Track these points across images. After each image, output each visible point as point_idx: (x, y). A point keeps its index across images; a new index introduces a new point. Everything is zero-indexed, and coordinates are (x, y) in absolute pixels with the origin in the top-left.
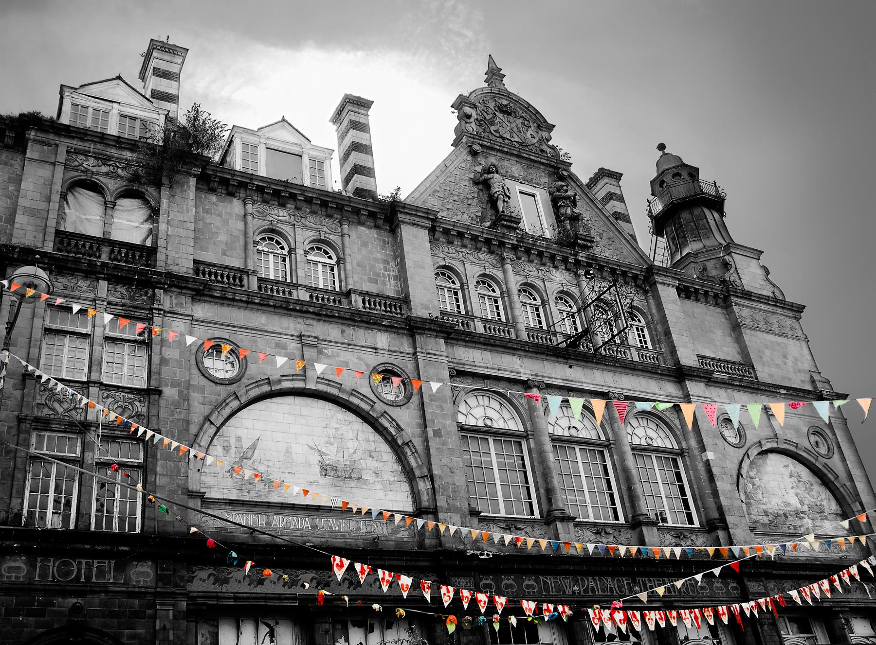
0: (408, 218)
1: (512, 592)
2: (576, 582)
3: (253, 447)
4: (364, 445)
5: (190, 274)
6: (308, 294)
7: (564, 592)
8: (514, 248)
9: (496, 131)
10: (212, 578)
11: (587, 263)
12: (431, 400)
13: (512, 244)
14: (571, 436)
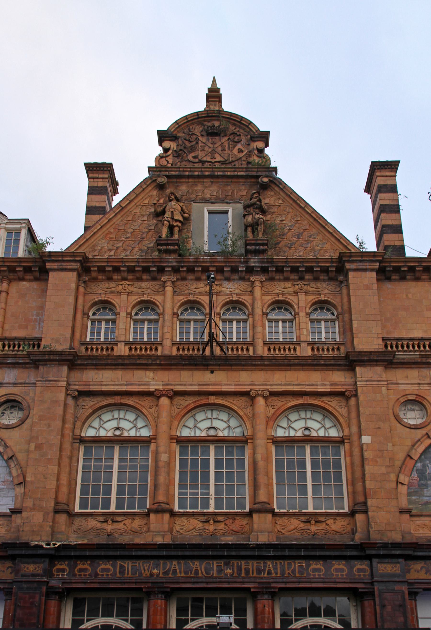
0: (55, 265)
1: (85, 575)
2: (157, 566)
5: (381, 348)
6: (127, 348)
7: (141, 574)
8: (176, 270)
9: (194, 157)
10: (424, 570)
11: (262, 267)
12: (40, 420)
13: (172, 267)
14: (209, 436)
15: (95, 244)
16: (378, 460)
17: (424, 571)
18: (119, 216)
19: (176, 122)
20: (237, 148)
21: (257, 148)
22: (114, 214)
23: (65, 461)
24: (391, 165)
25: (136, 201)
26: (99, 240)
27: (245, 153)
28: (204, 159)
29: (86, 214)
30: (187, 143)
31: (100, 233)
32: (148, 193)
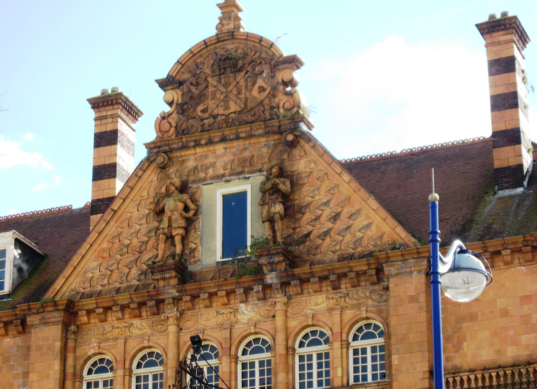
9: (203, 111)
15: (86, 269)
18: (112, 223)
19: (178, 61)
21: (283, 80)
22: (105, 223)
24: (505, 25)
25: (131, 197)
26: (91, 263)
27: (267, 92)
29: (94, 180)
30: (193, 89)
31: (90, 253)
32: (147, 179)
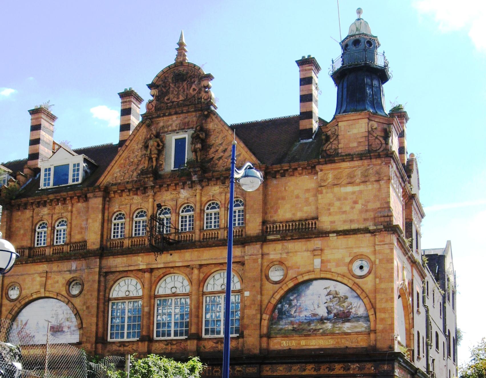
3: (26, 324)
4: (65, 315)
16: (252, 306)
17: (270, 371)
20: (192, 88)
23: (101, 314)
25: (134, 139)
28: (173, 100)
